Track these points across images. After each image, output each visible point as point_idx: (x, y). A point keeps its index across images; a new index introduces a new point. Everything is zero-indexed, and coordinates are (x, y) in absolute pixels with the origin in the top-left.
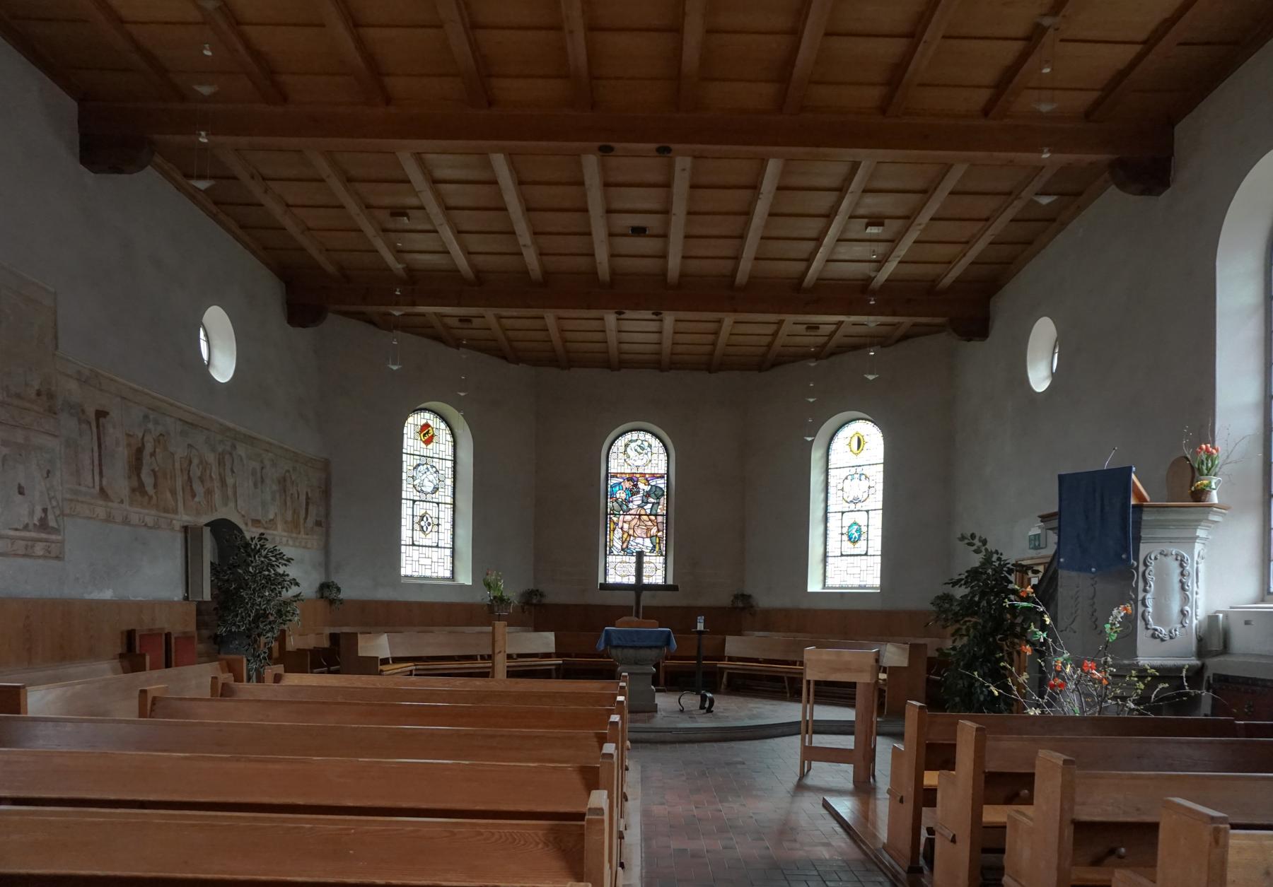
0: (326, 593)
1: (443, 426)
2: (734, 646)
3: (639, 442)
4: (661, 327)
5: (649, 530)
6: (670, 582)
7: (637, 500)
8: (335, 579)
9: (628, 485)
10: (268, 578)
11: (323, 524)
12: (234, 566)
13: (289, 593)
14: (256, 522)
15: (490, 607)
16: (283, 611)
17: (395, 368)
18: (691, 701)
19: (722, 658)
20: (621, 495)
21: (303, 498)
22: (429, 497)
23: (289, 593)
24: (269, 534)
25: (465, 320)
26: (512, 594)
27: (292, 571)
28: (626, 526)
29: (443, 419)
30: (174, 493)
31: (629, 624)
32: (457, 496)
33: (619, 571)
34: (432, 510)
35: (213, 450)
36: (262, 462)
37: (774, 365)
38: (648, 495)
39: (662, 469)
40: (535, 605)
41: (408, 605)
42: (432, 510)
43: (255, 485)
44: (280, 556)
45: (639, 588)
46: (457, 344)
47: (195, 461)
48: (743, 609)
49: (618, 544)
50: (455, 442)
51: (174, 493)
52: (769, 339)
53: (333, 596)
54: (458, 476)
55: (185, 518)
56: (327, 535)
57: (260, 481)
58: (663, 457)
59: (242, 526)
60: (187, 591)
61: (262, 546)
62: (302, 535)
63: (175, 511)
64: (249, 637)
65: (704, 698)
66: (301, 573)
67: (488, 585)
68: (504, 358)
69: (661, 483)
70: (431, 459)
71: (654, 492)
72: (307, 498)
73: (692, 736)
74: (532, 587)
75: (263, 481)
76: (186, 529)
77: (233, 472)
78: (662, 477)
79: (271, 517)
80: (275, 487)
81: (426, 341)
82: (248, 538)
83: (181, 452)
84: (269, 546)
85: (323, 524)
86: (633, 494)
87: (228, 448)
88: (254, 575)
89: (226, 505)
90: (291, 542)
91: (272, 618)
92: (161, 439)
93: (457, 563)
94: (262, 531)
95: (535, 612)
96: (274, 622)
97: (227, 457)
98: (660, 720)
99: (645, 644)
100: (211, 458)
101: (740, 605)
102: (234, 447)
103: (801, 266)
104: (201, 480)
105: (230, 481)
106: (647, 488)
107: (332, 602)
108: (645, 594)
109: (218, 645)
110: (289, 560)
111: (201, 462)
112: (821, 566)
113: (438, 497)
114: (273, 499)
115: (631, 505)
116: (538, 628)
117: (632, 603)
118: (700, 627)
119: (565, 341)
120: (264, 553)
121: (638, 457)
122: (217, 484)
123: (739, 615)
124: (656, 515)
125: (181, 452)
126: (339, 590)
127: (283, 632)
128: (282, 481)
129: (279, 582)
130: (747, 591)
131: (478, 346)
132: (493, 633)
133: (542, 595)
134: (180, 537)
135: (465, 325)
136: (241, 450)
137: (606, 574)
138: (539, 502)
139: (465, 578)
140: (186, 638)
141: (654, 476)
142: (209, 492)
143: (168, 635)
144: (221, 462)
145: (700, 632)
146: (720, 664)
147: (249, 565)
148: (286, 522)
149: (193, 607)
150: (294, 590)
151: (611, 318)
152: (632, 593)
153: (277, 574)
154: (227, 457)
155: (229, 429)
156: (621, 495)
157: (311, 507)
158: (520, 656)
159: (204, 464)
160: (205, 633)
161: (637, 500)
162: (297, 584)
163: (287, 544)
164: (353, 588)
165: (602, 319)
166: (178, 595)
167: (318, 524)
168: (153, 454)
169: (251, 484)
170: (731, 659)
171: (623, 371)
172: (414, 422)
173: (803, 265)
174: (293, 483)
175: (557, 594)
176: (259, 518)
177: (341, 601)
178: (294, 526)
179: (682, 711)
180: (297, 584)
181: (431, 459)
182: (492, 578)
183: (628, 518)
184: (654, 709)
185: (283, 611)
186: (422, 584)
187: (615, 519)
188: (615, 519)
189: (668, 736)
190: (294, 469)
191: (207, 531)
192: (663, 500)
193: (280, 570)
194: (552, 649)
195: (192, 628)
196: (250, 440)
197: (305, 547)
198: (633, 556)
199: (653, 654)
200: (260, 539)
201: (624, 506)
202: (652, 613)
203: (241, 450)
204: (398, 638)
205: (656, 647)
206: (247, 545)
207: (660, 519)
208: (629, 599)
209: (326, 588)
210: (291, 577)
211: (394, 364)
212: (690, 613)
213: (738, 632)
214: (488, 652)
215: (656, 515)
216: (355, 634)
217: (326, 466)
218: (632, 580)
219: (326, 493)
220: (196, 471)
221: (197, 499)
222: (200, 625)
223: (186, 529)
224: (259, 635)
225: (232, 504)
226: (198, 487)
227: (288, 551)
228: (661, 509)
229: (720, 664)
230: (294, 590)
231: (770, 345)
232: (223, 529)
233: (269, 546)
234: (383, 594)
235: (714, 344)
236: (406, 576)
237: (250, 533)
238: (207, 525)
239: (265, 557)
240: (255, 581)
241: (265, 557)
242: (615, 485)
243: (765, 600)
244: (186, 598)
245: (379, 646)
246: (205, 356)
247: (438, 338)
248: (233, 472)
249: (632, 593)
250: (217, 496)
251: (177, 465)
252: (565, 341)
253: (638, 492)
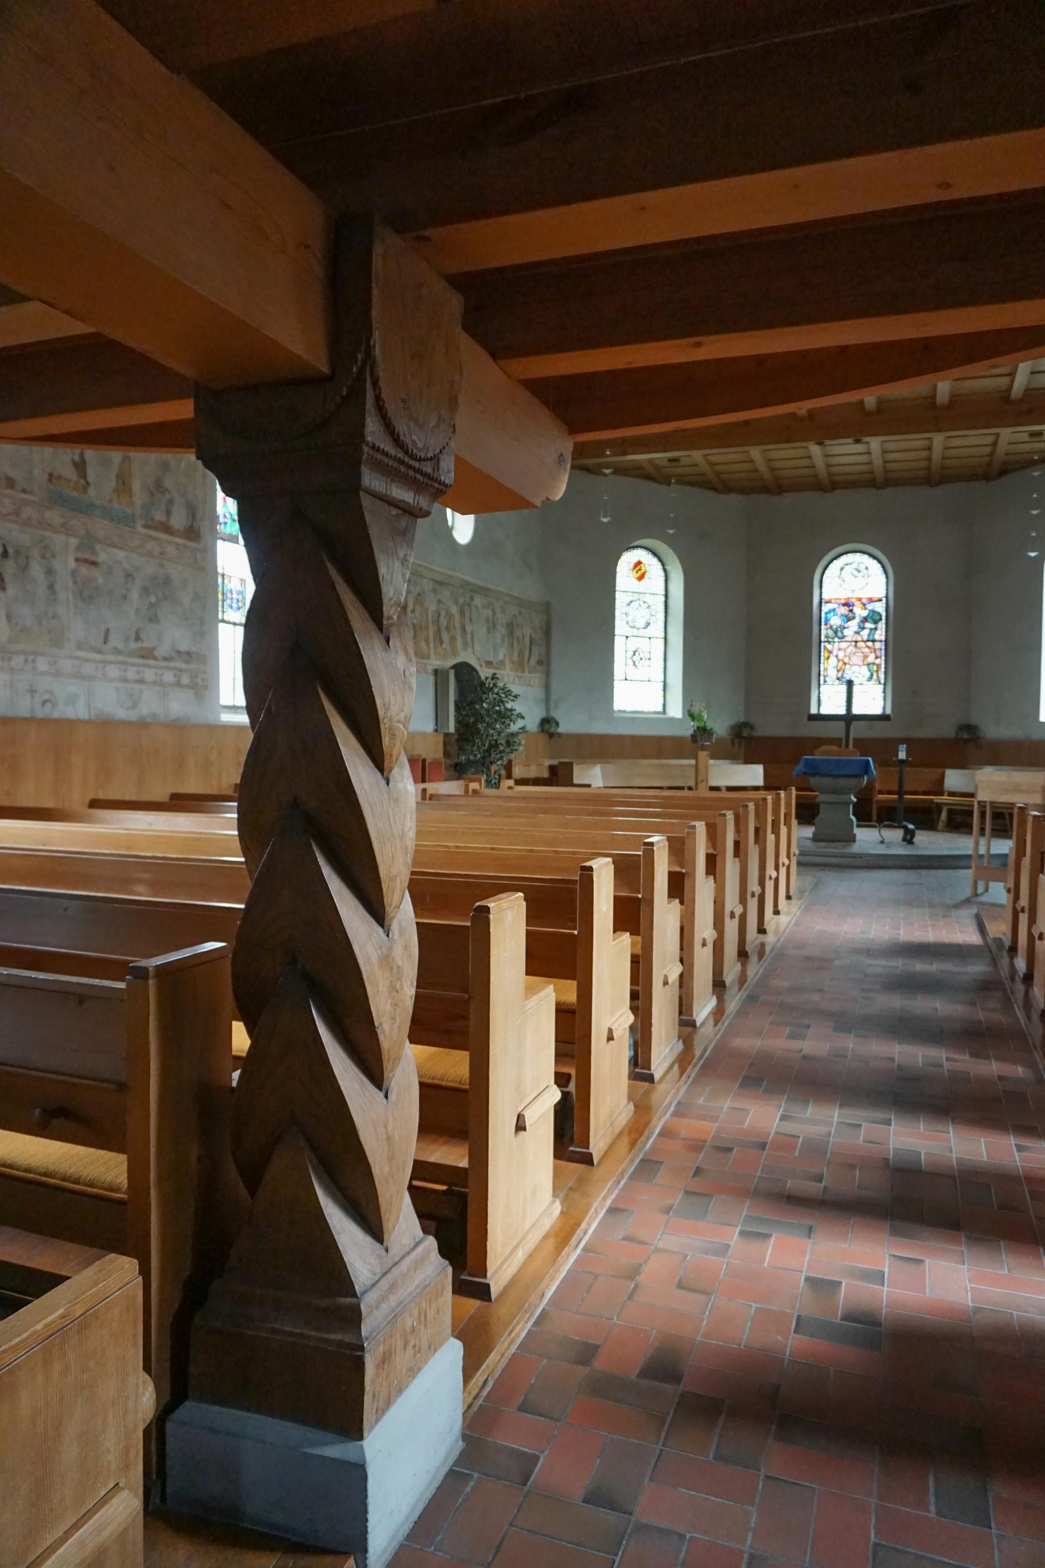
0: (547, 727)
1: (655, 561)
2: (954, 779)
3: (855, 565)
4: (869, 448)
5: (865, 657)
6: (888, 711)
7: (853, 625)
8: (557, 714)
9: (844, 610)
10: (499, 713)
11: (545, 663)
12: (472, 703)
13: (514, 728)
14: (489, 664)
15: (694, 737)
16: (511, 742)
17: (605, 520)
18: (897, 834)
19: (941, 794)
20: (835, 621)
21: (527, 639)
22: (642, 632)
23: (514, 728)
24: (500, 673)
25: (672, 460)
26: (720, 727)
27: (518, 706)
28: (841, 655)
29: (655, 554)
30: (427, 641)
31: (828, 753)
32: (669, 630)
33: (830, 700)
34: (643, 645)
35: (456, 602)
36: (493, 610)
37: (1003, 472)
38: (865, 620)
39: (881, 592)
40: (745, 738)
41: (620, 738)
42: (643, 645)
43: (488, 631)
44: (508, 693)
45: (849, 718)
46: (666, 481)
47: (443, 613)
48: (967, 741)
49: (832, 673)
50: (666, 576)
51: (427, 641)
52: (989, 449)
53: (552, 730)
54: (670, 611)
55: (435, 663)
56: (548, 674)
57: (492, 626)
58: (883, 579)
59: (478, 667)
60: (437, 724)
61: (495, 685)
62: (526, 674)
63: (428, 657)
64: (483, 765)
65: (907, 831)
66: (526, 710)
67: (692, 716)
68: (714, 489)
69: (880, 608)
70: (646, 596)
71: (874, 617)
72: (531, 639)
73: (889, 863)
74: (743, 720)
75: (494, 626)
76: (436, 672)
77: (471, 620)
78: (880, 600)
79: (501, 657)
80: (504, 631)
81: (638, 481)
82: (483, 678)
83: (432, 607)
84: (500, 684)
85: (545, 663)
86: (849, 620)
87: (468, 600)
88: (488, 710)
89: (465, 649)
90: (517, 681)
91: (502, 748)
92: (419, 598)
93: (668, 697)
94: (494, 671)
95: (744, 744)
96: (503, 751)
97: (466, 608)
98: (856, 848)
99: (843, 772)
100: (454, 610)
101: (966, 736)
102: (472, 599)
103: (1005, 381)
104: (448, 629)
105: (469, 628)
106: (865, 613)
107: (551, 735)
108: (854, 725)
109: (458, 771)
110: (516, 696)
111: (447, 614)
112: (668, 681)
113: (649, 632)
114: (503, 641)
115: (846, 632)
116: (749, 760)
117: (842, 735)
118: (902, 755)
119: (773, 470)
120: (496, 690)
121: (854, 581)
122: (459, 632)
123: (968, 746)
124: (874, 641)
125: (432, 607)
126: (557, 724)
127: (510, 761)
128: (510, 626)
129: (506, 716)
130: (973, 721)
131: (686, 481)
132: (696, 766)
133: (752, 727)
134: (431, 679)
135: (674, 464)
136: (478, 601)
137: (819, 705)
138: (751, 633)
139: (676, 711)
140: (436, 764)
141: (871, 600)
142: (453, 639)
143: (424, 761)
144: (462, 613)
145: (902, 761)
146: (937, 799)
147: (483, 701)
148: (513, 663)
149: (441, 738)
150: (520, 723)
151: (815, 449)
152: (842, 724)
153: (506, 709)
154: (466, 608)
155: (468, 583)
156: (835, 621)
157: (533, 648)
158: (730, 789)
159: (450, 616)
160: (449, 762)
161: (853, 625)
162: (523, 718)
163: (514, 682)
164: (572, 722)
165: (806, 447)
166: (430, 727)
167: (540, 662)
168: (413, 611)
169: (485, 629)
170: (952, 794)
171: (838, 492)
172: (627, 560)
173: (1005, 381)
174: (518, 625)
175: (770, 727)
176: (491, 660)
177: (559, 735)
178: (520, 666)
179: (882, 842)
180: (523, 718)
181: (646, 596)
182: (695, 710)
183: (843, 645)
184: (852, 839)
185: (511, 742)
186: (634, 718)
187: (829, 647)
188: (829, 647)
189: (858, 862)
190: (520, 613)
191: (452, 673)
192: (882, 625)
193: (509, 706)
194: (760, 782)
195: (440, 755)
196: (484, 591)
197: (529, 685)
198: (849, 683)
199: (853, 781)
200: (493, 678)
201: (838, 633)
202: (864, 745)
203: (478, 601)
204: (610, 767)
205: (855, 776)
206: (482, 684)
207: (878, 645)
208: (837, 730)
209: (547, 723)
210: (517, 712)
211: (605, 516)
212: (892, 744)
213: (962, 766)
214: (692, 784)
215: (874, 641)
216: (572, 763)
217: (547, 609)
218: (842, 711)
219: (547, 632)
220: (443, 622)
221: (444, 646)
222: (447, 754)
223: (436, 672)
224: (491, 763)
225: (470, 649)
226: (445, 637)
227: (515, 689)
228: (880, 634)
229: (937, 799)
230: (520, 723)
231: (992, 454)
232: (463, 670)
233: (500, 684)
234: (599, 728)
235: (929, 459)
236: (619, 711)
237: (484, 673)
238: (451, 668)
239: (497, 694)
240: (488, 715)
241: (497, 694)
242: (829, 612)
243: (992, 730)
244: (436, 731)
245: (594, 776)
246: (450, 523)
247: (649, 478)
248: (471, 620)
249: (842, 724)
250: (459, 642)
251: (430, 619)
252: (773, 470)
253: (854, 618)
